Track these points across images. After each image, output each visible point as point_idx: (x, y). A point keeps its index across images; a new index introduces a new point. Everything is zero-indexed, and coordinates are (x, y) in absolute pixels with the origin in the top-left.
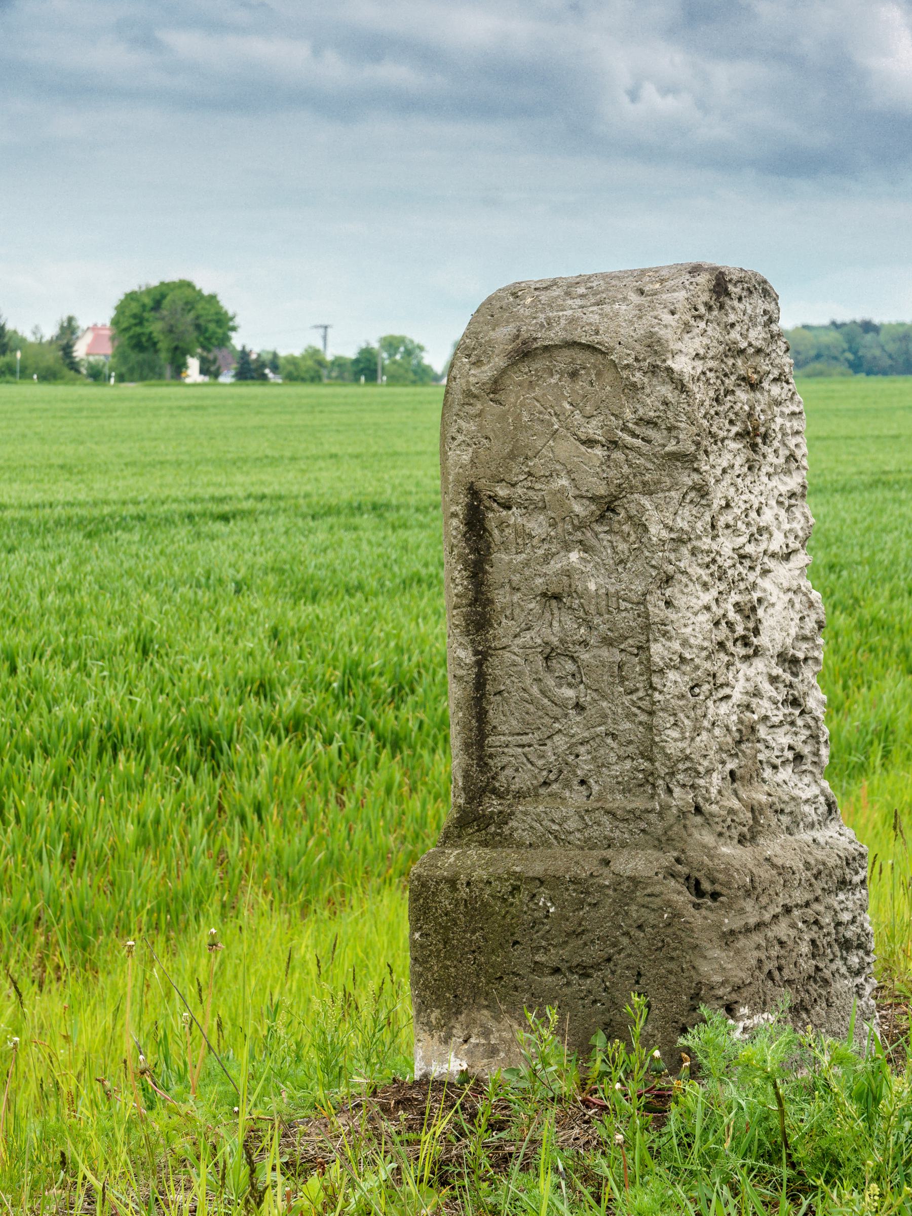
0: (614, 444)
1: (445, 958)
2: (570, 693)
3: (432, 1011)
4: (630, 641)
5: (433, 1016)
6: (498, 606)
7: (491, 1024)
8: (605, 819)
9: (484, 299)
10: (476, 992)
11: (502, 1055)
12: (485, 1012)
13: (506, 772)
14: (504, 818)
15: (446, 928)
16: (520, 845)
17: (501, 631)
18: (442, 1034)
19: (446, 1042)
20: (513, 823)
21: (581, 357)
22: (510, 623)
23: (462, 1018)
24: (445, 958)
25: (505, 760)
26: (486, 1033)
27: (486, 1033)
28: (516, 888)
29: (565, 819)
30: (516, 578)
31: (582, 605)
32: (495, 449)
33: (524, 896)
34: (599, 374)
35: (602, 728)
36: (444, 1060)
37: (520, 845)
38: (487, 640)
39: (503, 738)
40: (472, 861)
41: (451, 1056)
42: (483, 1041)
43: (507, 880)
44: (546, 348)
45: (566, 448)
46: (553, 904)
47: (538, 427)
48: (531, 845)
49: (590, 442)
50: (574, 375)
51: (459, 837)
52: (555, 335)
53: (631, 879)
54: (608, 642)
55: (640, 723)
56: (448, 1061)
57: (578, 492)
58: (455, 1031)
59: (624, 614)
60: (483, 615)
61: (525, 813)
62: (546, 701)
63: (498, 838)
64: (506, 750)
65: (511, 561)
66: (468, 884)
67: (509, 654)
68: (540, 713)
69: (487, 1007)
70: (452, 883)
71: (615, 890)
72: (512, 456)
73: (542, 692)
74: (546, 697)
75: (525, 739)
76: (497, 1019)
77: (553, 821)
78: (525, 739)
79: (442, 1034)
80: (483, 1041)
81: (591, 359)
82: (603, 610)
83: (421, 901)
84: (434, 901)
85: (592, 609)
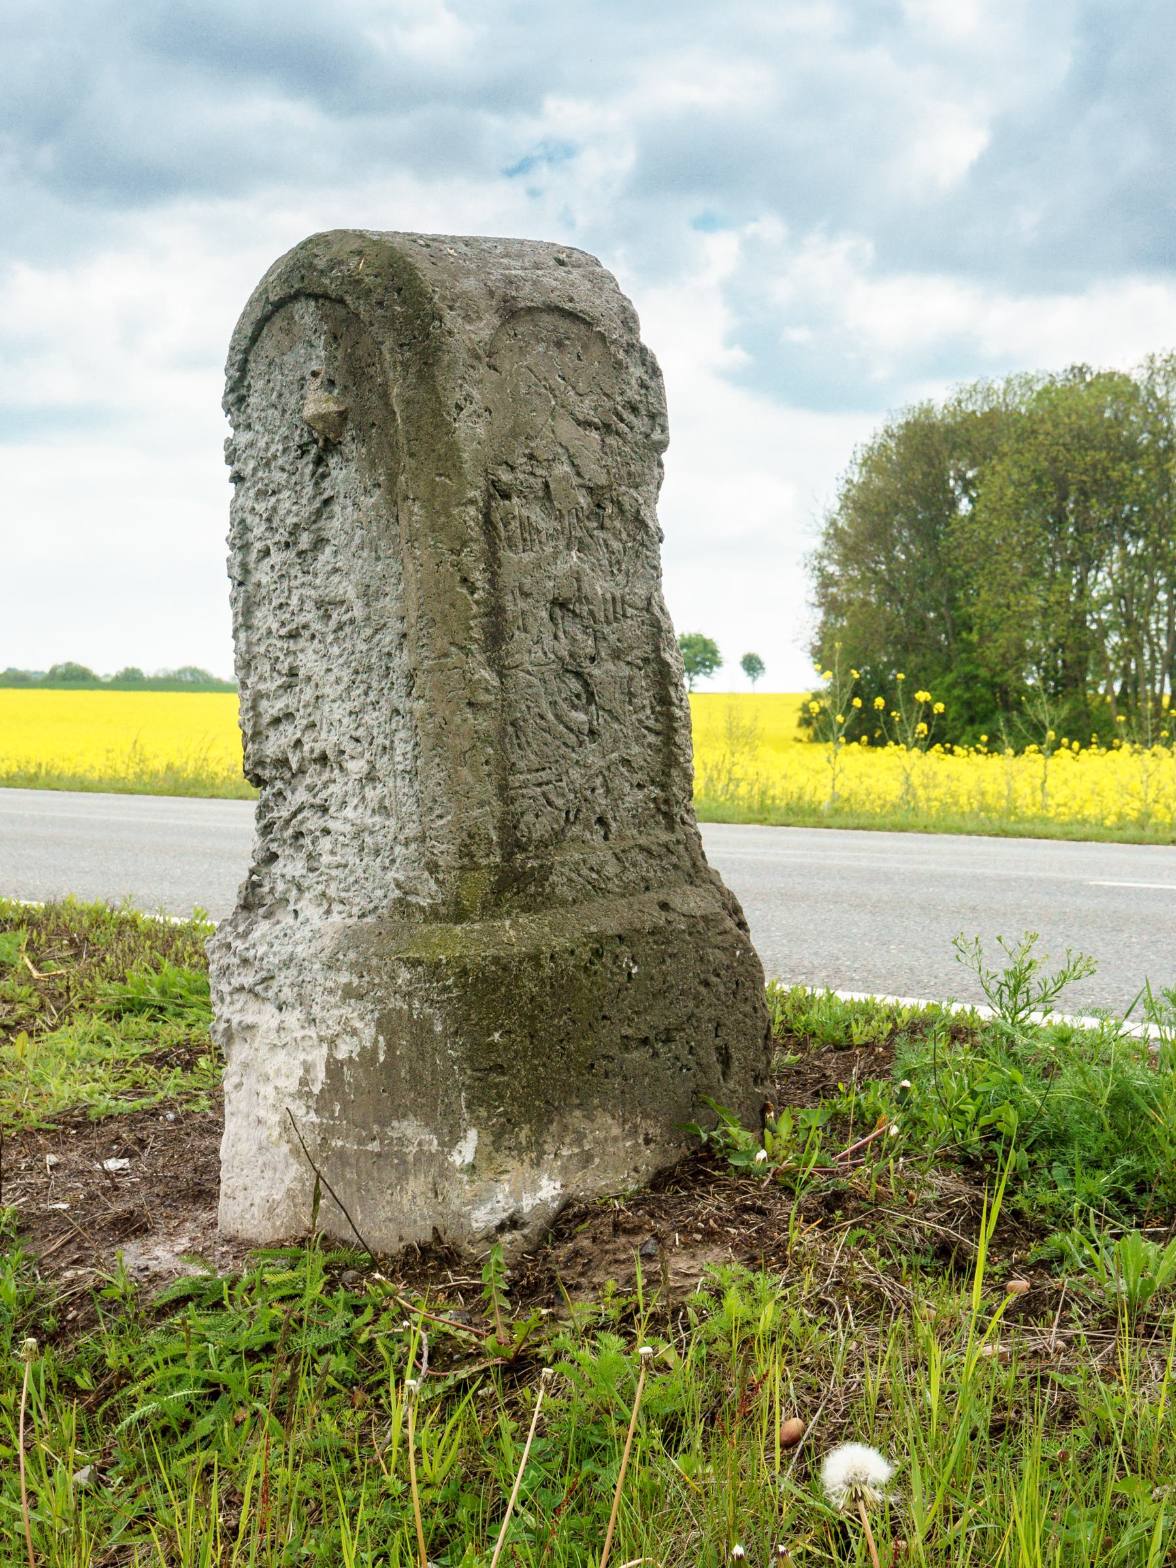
0: (607, 427)
1: (533, 1056)
2: (582, 717)
3: (521, 1129)
4: (636, 652)
5: (522, 1136)
6: (509, 616)
7: (584, 1125)
8: (640, 857)
9: (303, 238)
10: (568, 1090)
11: (597, 1160)
12: (577, 1113)
13: (526, 818)
14: (546, 871)
15: (533, 1018)
16: (563, 903)
17: (512, 646)
18: (533, 1155)
19: (538, 1165)
20: (553, 878)
21: (564, 325)
22: (523, 635)
23: (554, 1128)
24: (533, 1056)
25: (526, 802)
26: (579, 1139)
27: (579, 1139)
28: (597, 954)
29: (603, 864)
30: (527, 582)
31: (591, 613)
32: (496, 423)
33: (607, 960)
34: (585, 347)
35: (615, 755)
36: (535, 1187)
37: (563, 903)
38: (500, 658)
39: (522, 777)
40: (514, 932)
41: (544, 1182)
42: (576, 1150)
43: (585, 945)
44: (530, 310)
45: (566, 429)
46: (635, 962)
47: (537, 401)
48: (574, 901)
49: (587, 424)
50: (559, 344)
51: (497, 905)
52: (539, 300)
53: (704, 918)
54: (617, 655)
55: (650, 745)
56: (541, 1188)
57: (580, 481)
58: (546, 1147)
59: (629, 621)
60: (496, 625)
61: (563, 864)
62: (561, 727)
63: (539, 899)
64: (524, 791)
65: (520, 562)
66: (552, 957)
67: (522, 674)
68: (558, 742)
69: (579, 1106)
70: (535, 958)
71: (690, 934)
72: (514, 434)
73: (557, 716)
74: (562, 722)
75: (544, 776)
76: (590, 1118)
77: (592, 869)
78: (544, 776)
79: (533, 1155)
80: (576, 1150)
81: (575, 329)
82: (611, 617)
83: (503, 989)
84: (518, 987)
85: (601, 616)
